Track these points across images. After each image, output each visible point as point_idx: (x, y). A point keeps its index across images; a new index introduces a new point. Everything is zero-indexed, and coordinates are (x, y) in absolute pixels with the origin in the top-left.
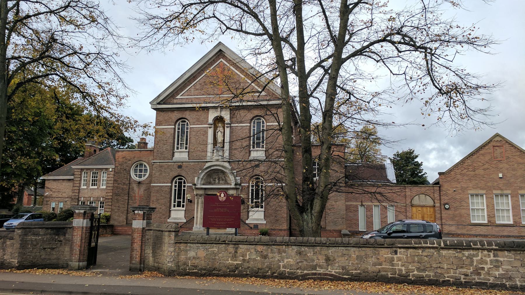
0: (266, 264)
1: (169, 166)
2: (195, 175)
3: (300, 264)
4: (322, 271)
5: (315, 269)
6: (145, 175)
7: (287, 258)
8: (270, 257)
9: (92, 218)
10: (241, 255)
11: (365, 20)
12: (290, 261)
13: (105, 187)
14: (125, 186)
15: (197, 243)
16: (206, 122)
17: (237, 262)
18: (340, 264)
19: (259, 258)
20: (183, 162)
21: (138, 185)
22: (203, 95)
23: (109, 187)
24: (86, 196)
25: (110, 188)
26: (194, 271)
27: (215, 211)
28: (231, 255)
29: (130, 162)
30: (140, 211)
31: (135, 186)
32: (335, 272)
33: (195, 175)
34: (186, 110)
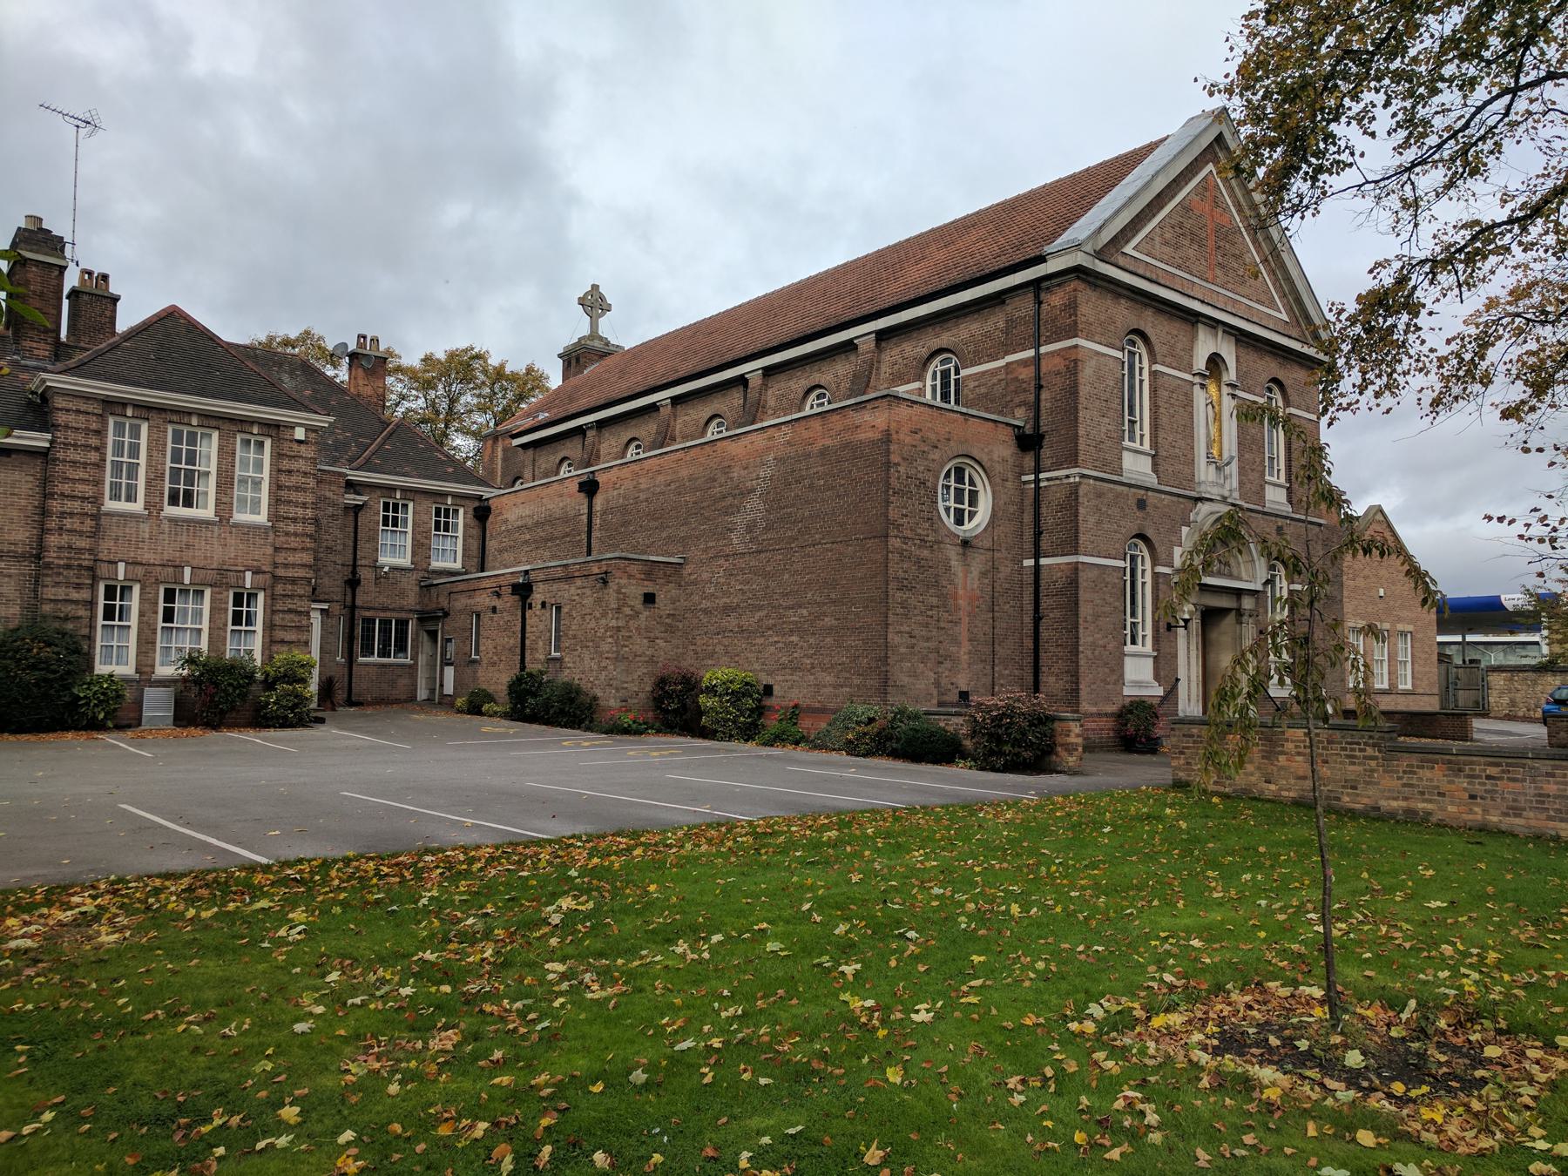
11: (1223, 82)
13: (262, 518)
21: (960, 550)
23: (295, 520)
24: (148, 557)
25: (299, 528)
29: (936, 455)
31: (953, 553)
34: (1118, 296)
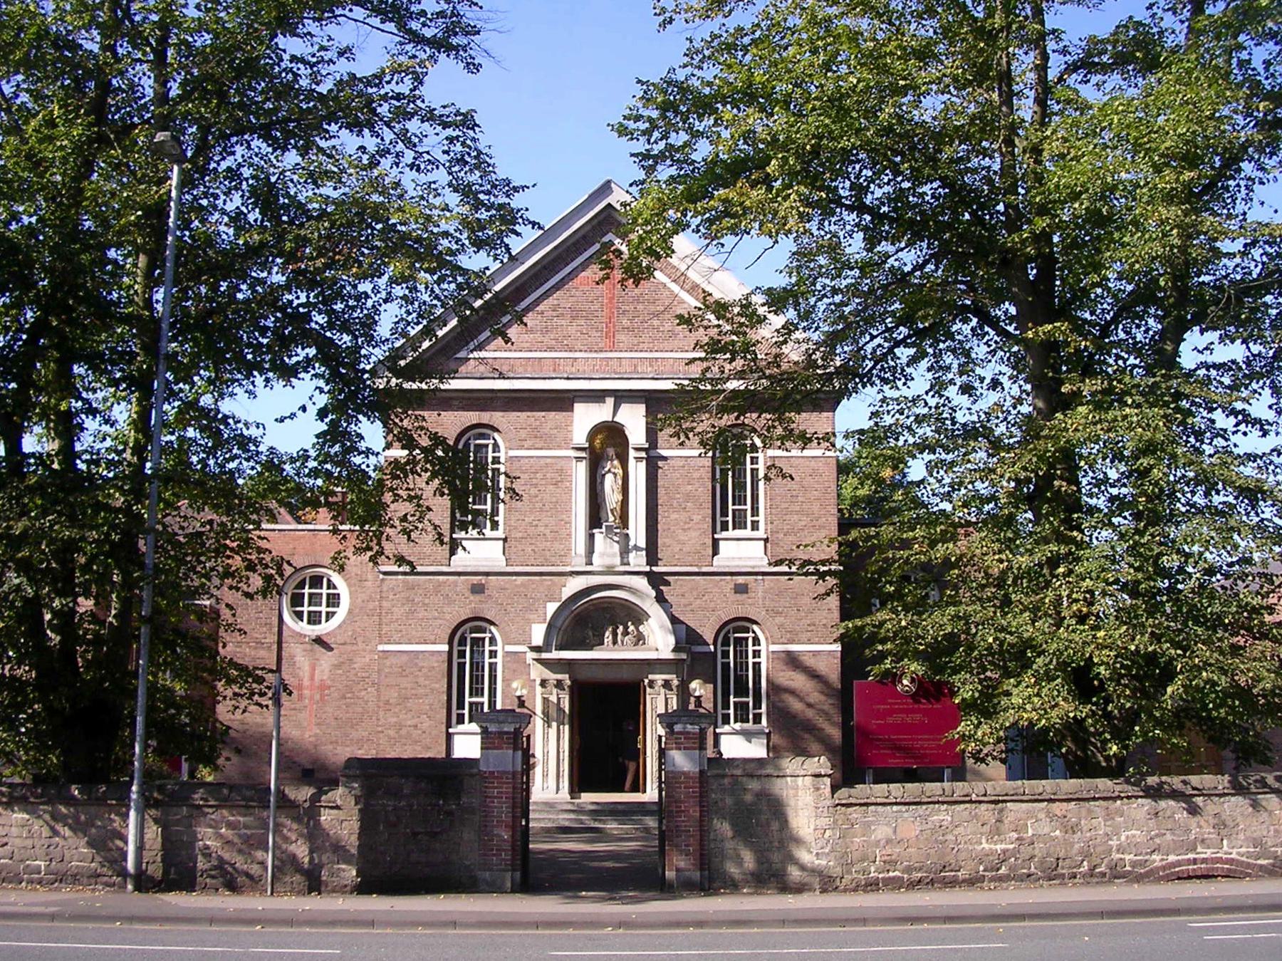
0: (1077, 846)
1: (440, 584)
2: (531, 617)
3: (1158, 841)
4: (1208, 853)
5: (1194, 849)
6: (329, 616)
7: (1127, 829)
8: (1085, 828)
9: (215, 764)
10: (1013, 827)
12: (1134, 836)
14: (262, 653)
15: (896, 804)
16: (566, 443)
17: (1003, 846)
18: (1248, 834)
19: (1058, 832)
20: (487, 574)
22: (551, 349)
26: (891, 874)
27: (890, 720)
28: (987, 828)
30: (689, 726)
32: (1238, 854)
33: (531, 617)
